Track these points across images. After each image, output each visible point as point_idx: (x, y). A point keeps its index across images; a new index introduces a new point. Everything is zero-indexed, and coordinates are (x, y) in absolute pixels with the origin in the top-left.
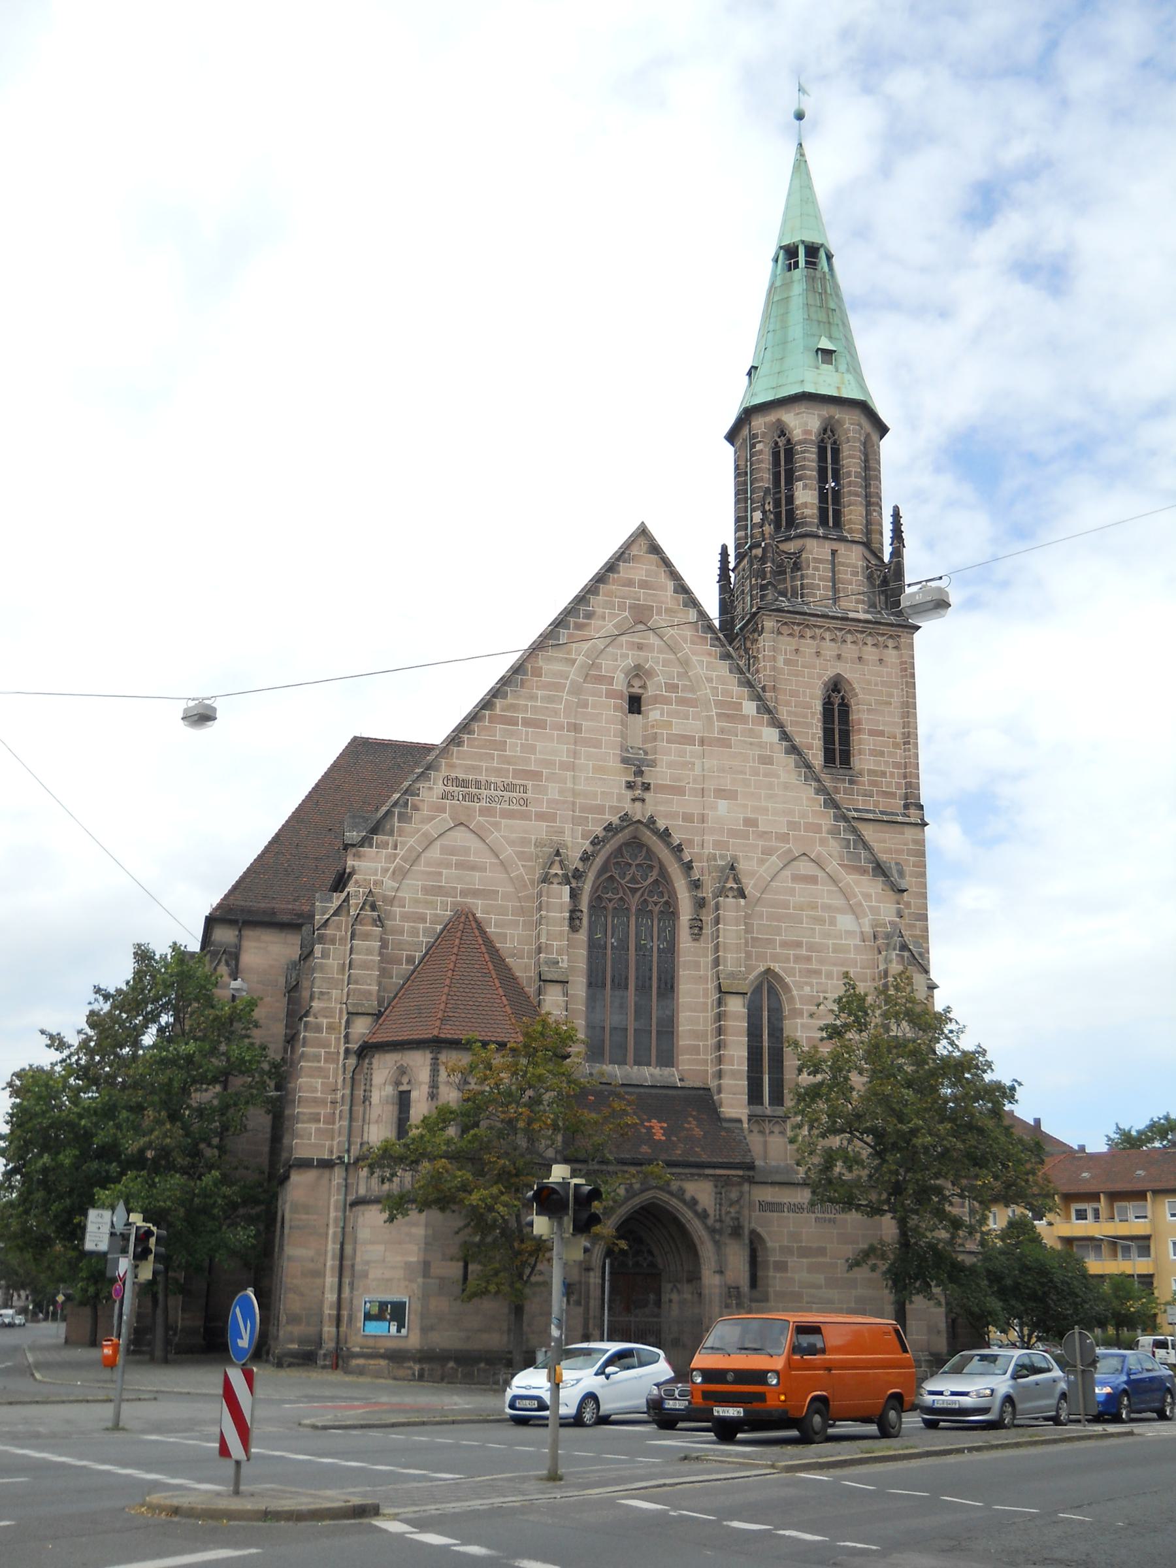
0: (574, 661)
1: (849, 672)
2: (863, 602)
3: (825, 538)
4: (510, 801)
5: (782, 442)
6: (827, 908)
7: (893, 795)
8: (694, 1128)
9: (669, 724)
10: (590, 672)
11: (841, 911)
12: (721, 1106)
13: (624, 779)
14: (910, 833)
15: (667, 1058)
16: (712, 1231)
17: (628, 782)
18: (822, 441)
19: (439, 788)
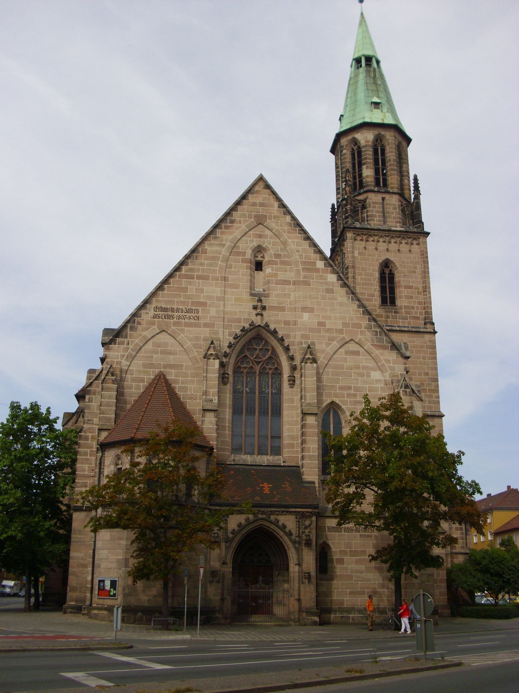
0: (224, 245)
1: (392, 257)
2: (400, 222)
3: (378, 192)
4: (190, 318)
5: (355, 148)
6: (364, 368)
7: (418, 318)
8: (287, 486)
9: (277, 275)
10: (234, 250)
11: (374, 369)
12: (303, 475)
13: (252, 304)
14: (427, 337)
15: (277, 451)
16: (294, 542)
17: (254, 306)
18: (376, 145)
19: (152, 313)
